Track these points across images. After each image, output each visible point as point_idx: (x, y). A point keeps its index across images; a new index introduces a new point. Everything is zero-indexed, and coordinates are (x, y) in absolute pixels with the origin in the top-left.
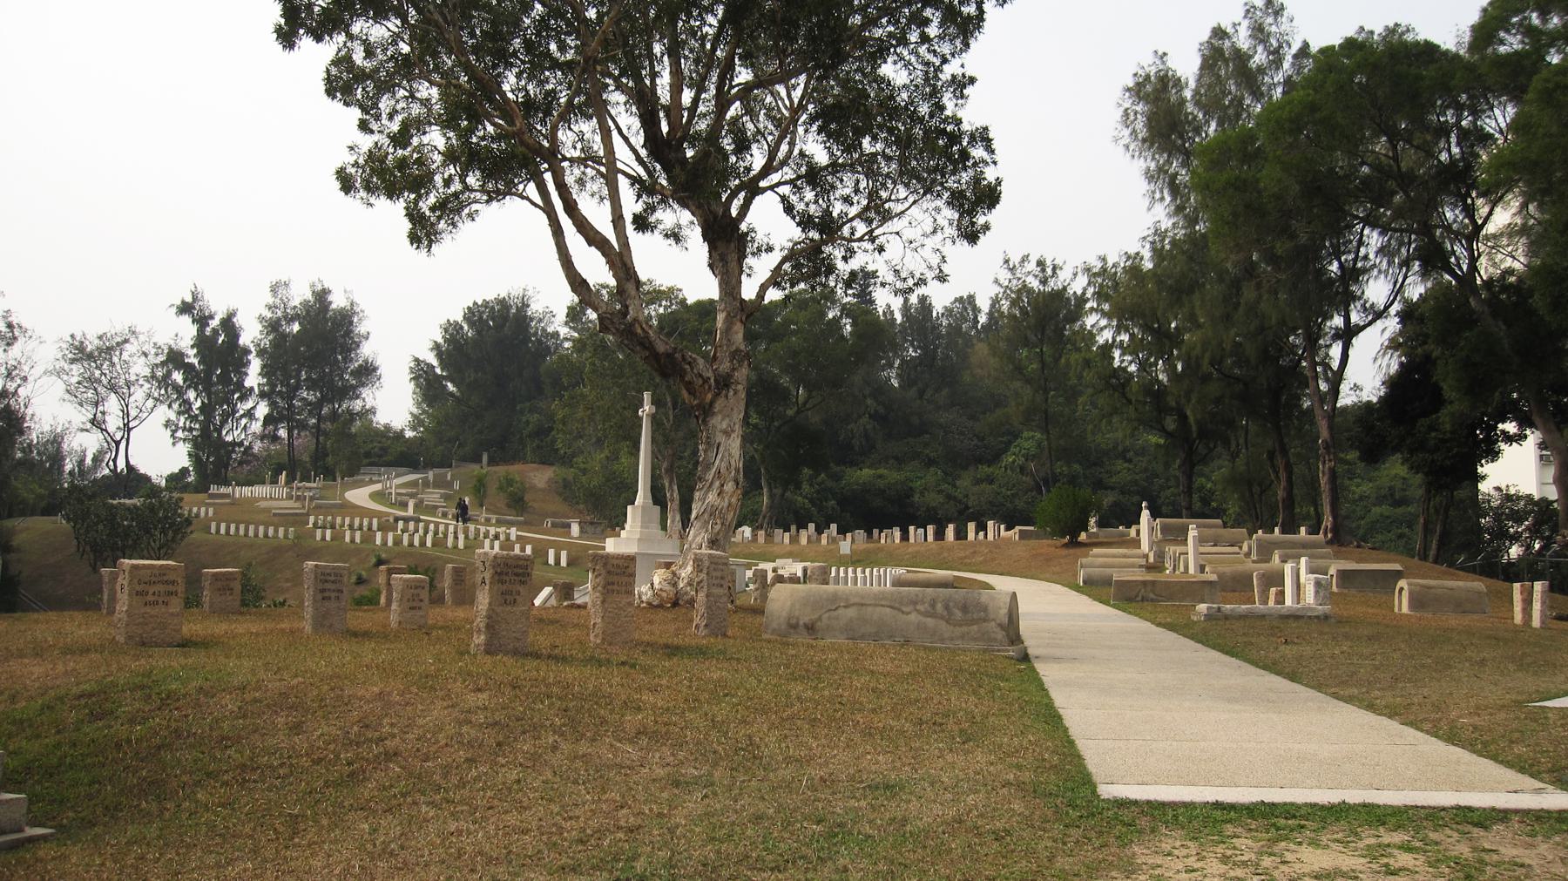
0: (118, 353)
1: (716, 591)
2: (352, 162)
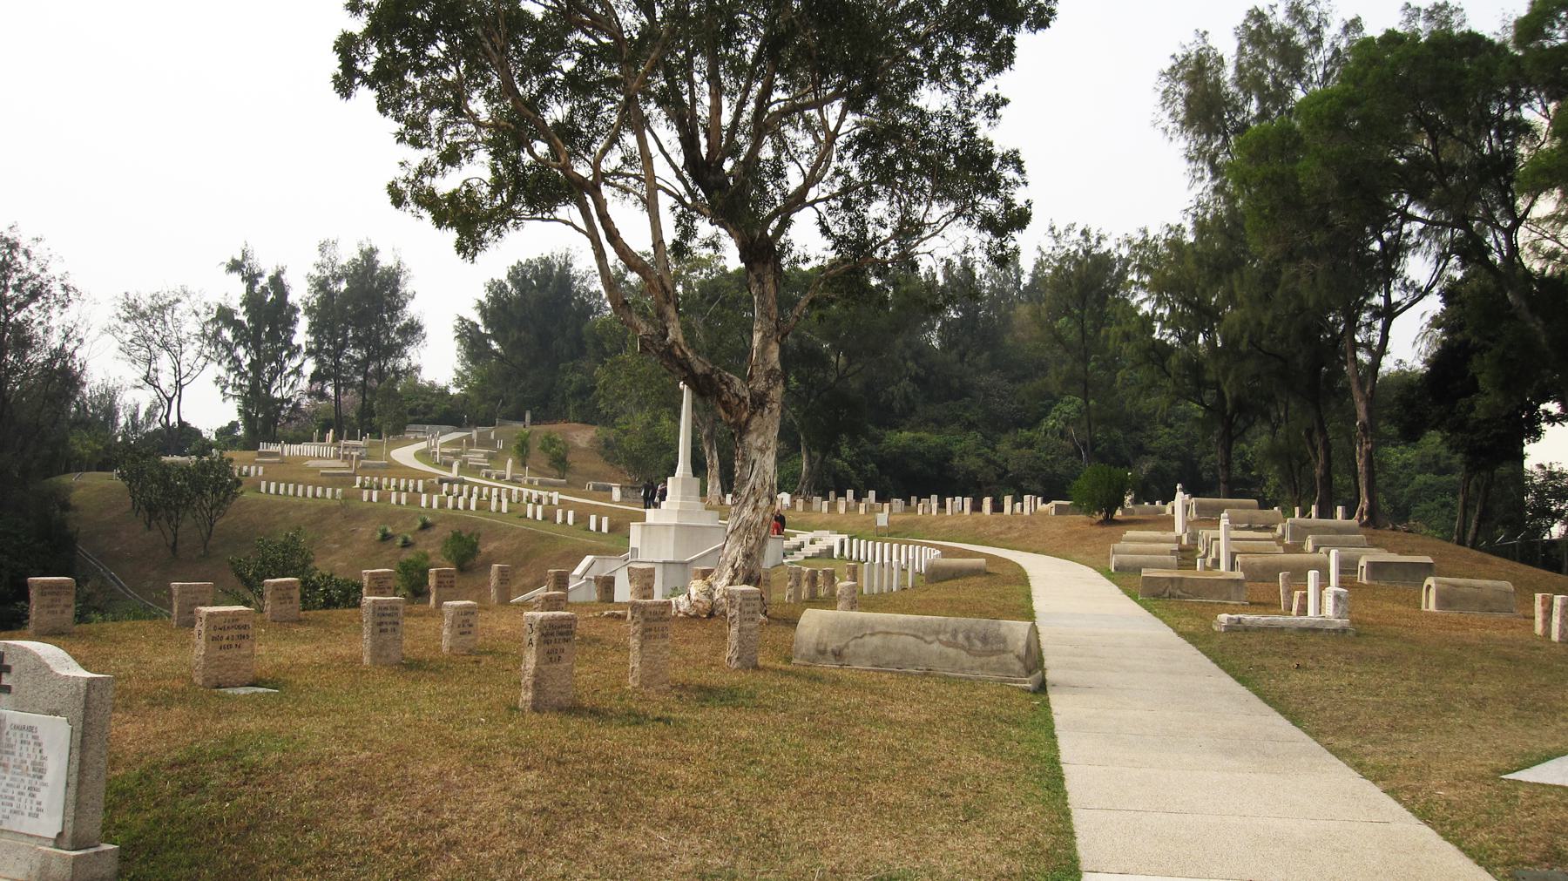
0: (170, 312)
1: (747, 625)
2: (403, 178)
